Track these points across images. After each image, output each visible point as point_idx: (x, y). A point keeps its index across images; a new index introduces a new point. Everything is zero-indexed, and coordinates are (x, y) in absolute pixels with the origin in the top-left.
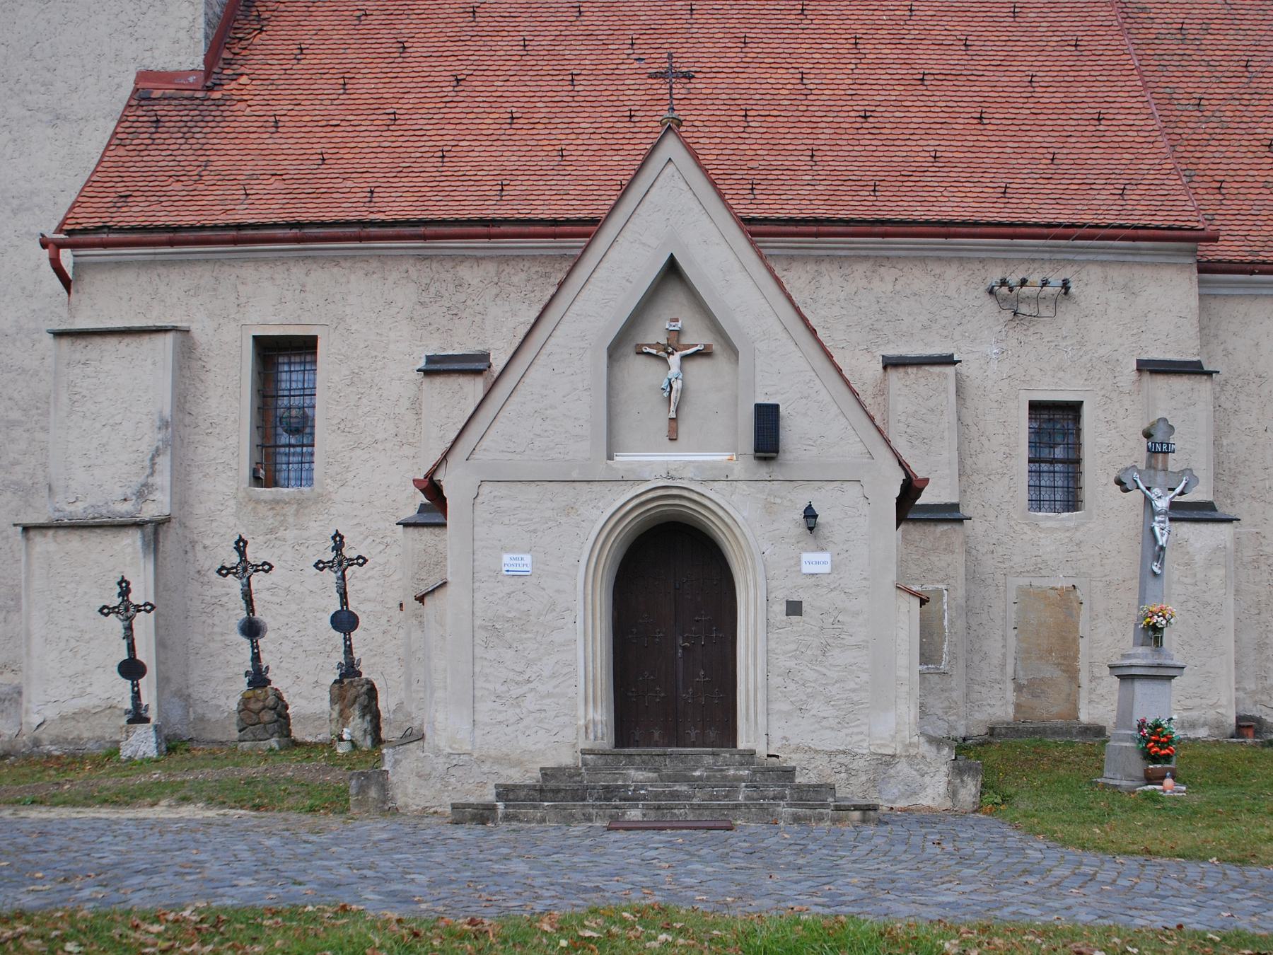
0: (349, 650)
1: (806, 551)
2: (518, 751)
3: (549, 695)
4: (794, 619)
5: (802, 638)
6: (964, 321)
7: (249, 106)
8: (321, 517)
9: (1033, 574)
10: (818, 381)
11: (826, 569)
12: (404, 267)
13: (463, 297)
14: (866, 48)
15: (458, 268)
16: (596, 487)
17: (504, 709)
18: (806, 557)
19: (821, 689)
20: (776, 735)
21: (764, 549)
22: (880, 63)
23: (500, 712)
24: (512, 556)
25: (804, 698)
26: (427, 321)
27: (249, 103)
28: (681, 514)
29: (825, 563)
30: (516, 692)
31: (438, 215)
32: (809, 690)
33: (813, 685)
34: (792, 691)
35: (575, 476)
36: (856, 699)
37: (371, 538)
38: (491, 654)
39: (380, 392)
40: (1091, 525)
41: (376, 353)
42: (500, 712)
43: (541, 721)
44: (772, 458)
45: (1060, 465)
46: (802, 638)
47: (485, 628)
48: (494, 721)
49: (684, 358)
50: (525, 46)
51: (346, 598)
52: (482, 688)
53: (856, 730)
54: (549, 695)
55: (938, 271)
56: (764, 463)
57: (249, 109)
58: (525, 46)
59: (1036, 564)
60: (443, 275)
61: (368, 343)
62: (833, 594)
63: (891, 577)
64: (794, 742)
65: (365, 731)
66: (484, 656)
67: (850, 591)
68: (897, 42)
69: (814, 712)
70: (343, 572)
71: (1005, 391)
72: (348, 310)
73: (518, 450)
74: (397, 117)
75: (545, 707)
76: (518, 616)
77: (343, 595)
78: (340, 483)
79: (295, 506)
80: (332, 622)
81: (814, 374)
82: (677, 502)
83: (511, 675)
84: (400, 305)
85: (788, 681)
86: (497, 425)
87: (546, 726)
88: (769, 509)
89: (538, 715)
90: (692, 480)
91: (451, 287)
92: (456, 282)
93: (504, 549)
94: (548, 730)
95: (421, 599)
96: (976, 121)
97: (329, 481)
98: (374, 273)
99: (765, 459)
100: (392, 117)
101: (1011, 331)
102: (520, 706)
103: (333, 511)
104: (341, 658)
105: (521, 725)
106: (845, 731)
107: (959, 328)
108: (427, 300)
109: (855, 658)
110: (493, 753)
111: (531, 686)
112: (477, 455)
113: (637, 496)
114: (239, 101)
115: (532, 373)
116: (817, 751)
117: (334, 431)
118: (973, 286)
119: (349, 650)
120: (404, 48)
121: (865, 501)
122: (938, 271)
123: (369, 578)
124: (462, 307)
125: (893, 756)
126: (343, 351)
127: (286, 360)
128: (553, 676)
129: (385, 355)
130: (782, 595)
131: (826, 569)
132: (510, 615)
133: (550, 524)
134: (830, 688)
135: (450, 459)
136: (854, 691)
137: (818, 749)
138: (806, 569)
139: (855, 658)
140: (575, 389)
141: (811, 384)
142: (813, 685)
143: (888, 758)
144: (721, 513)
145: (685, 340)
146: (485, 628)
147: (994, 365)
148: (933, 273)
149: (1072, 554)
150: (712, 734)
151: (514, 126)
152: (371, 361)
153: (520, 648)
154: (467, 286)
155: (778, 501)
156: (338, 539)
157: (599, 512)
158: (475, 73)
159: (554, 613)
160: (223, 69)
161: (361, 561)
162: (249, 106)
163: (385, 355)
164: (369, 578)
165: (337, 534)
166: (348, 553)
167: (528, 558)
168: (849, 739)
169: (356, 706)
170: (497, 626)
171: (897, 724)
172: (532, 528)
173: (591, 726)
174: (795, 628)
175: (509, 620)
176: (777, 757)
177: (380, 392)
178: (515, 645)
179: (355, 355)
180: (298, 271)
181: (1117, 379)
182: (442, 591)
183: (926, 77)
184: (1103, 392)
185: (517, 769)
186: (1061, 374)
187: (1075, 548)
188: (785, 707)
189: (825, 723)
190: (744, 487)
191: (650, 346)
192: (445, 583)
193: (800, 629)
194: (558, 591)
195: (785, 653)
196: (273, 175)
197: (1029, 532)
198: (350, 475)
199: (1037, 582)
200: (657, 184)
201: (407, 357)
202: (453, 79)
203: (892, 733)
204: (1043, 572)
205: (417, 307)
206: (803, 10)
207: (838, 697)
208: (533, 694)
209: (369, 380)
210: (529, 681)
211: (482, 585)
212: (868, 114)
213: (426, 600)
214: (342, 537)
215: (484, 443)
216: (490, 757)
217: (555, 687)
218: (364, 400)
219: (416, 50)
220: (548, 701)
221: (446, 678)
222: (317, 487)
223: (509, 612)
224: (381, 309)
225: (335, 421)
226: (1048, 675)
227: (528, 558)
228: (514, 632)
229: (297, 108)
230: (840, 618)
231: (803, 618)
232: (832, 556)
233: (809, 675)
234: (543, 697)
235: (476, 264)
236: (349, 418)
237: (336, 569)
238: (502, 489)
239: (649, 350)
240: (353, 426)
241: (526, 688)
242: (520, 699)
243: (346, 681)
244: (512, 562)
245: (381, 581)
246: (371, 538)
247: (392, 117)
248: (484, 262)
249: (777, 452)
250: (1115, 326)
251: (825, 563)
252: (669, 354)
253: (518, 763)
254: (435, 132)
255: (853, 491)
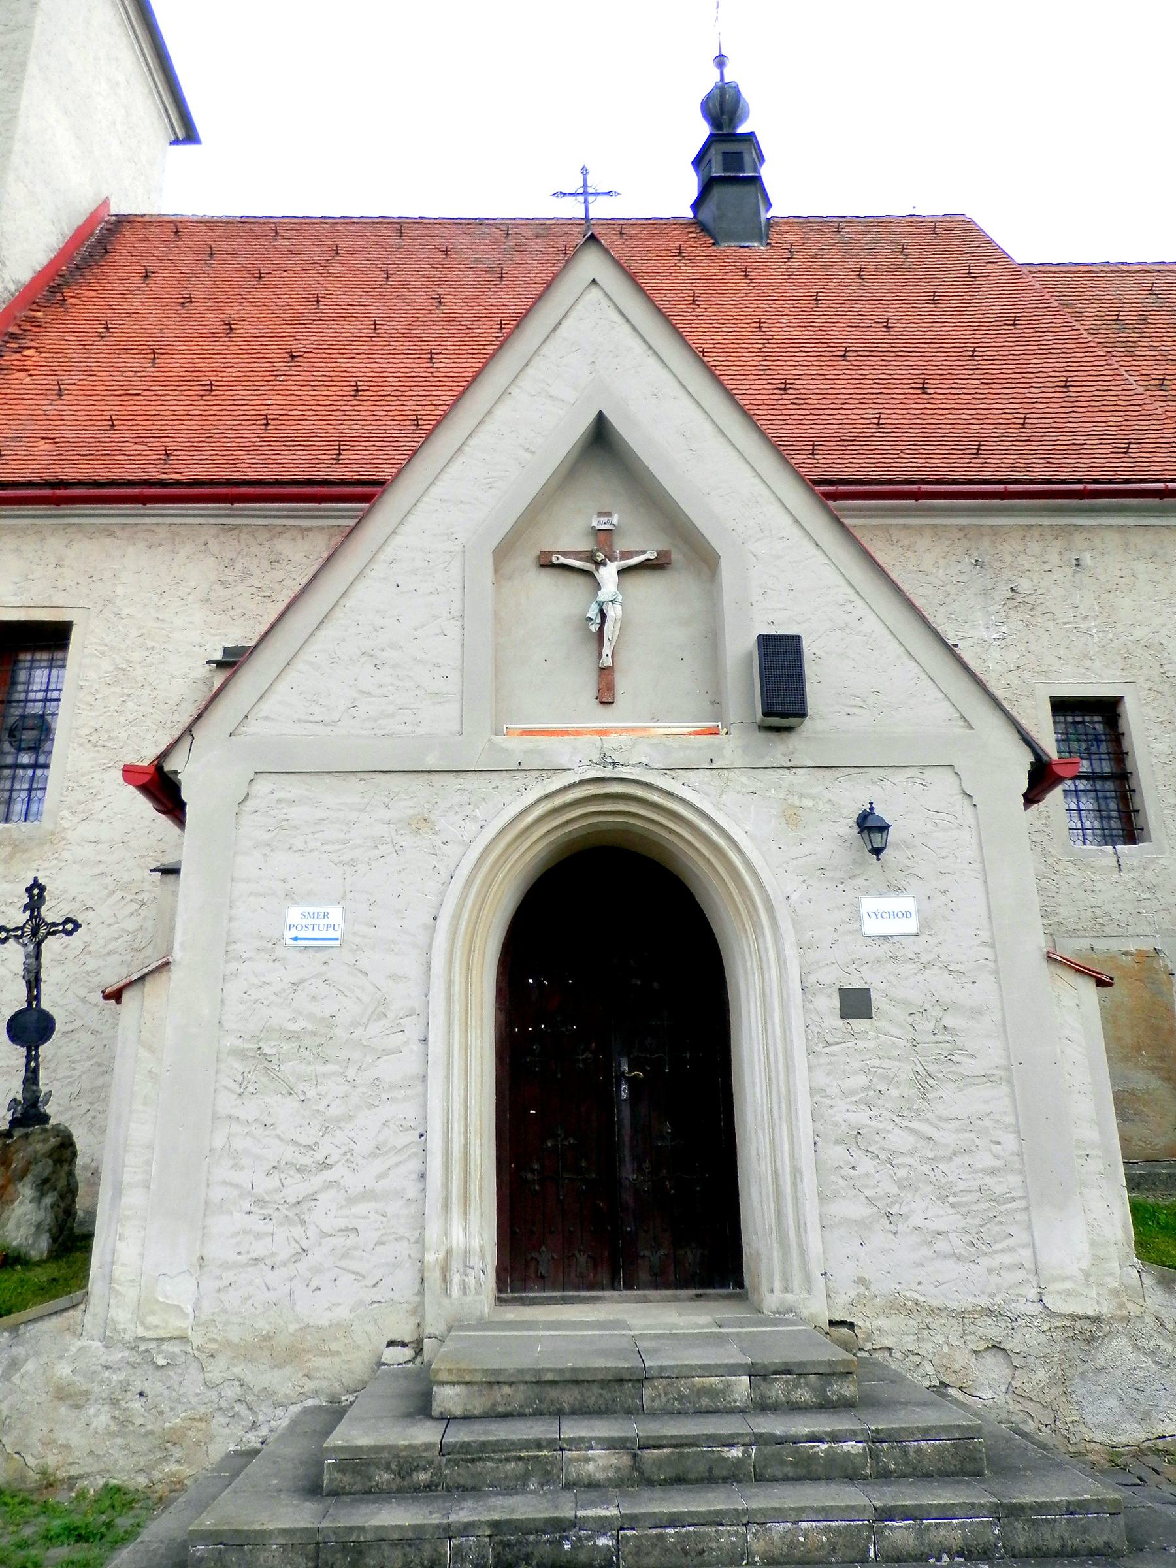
0: (31, 1077)
1: (866, 892)
2: (292, 1328)
3: (367, 1195)
4: (859, 1024)
5: (876, 1062)
6: (948, 600)
7: (30, 375)
8: (46, 864)
9: (1093, 933)
10: (859, 603)
11: (910, 926)
12: (203, 539)
13: (280, 575)
14: (770, 329)
15: (275, 541)
16: (471, 781)
17: (268, 1227)
18: (869, 904)
19: (926, 1169)
20: (845, 1273)
21: (788, 890)
22: (790, 343)
23: (259, 1236)
24: (306, 910)
25: (894, 1190)
26: (230, 604)
27: (31, 372)
28: (626, 832)
29: (906, 915)
30: (297, 1188)
31: (251, 475)
32: (902, 1173)
33: (909, 1160)
34: (867, 1175)
35: (431, 762)
36: (999, 1190)
37: (120, 894)
38: (250, 1110)
39: (154, 694)
40: (1162, 862)
41: (153, 644)
42: (259, 1236)
43: (345, 1255)
44: (789, 729)
45: (1085, 782)
46: (876, 1062)
47: (240, 1054)
48: (243, 1259)
49: (622, 572)
50: (375, 329)
51: (38, 987)
52: (225, 1183)
53: (1007, 1259)
54: (367, 1195)
55: (906, 542)
56: (772, 736)
57: (29, 378)
58: (375, 329)
59: (1095, 918)
60: (255, 549)
61: (144, 631)
62: (928, 972)
63: (1038, 942)
64: (884, 1286)
65: (38, 1226)
66: (235, 1112)
67: (960, 968)
68: (807, 324)
69: (917, 1220)
70: (38, 945)
71: (1015, 686)
72: (120, 590)
73: (327, 719)
74: (214, 388)
75: (355, 1223)
76: (310, 1027)
77: (34, 982)
78: (83, 816)
79: (9, 849)
80: (10, 1028)
81: (850, 591)
82: (621, 807)
83: (289, 1153)
84: (193, 584)
85: (857, 1153)
86: (291, 676)
87: (355, 1266)
88: (792, 817)
89: (338, 1241)
90: (649, 768)
91: (265, 563)
92: (273, 558)
93: (290, 896)
94: (359, 1275)
95: (116, 996)
96: (919, 391)
97: (65, 813)
98: (160, 545)
99: (778, 730)
100: (209, 388)
101: (1013, 611)
102: (303, 1223)
103: (66, 855)
104: (15, 1088)
105: (303, 1266)
106: (985, 1262)
107: (942, 609)
108: (231, 579)
109: (986, 1102)
110: (234, 1336)
111: (328, 1175)
112: (253, 727)
113: (547, 797)
114: (18, 371)
115: (360, 590)
116: (934, 1312)
117: (81, 745)
118: (954, 558)
119: (31, 1077)
120: (231, 329)
121: (966, 802)
122: (906, 542)
123: (109, 953)
124: (278, 587)
125: (1096, 1320)
126: (107, 640)
127: (29, 657)
128: (378, 1151)
129: (165, 646)
130: (835, 977)
131: (910, 926)
132: (293, 1027)
133: (383, 849)
134: (944, 1167)
135: (199, 733)
136: (993, 1172)
137: (934, 1303)
138: (872, 927)
139: (986, 1102)
140: (435, 617)
141: (849, 607)
142: (909, 1160)
143: (1086, 1326)
144: (705, 826)
145: (620, 545)
146: (240, 1054)
147: (995, 654)
148: (900, 544)
149: (1143, 904)
150: (691, 1255)
151: (358, 398)
152: (147, 653)
153: (311, 1094)
154: (286, 562)
155: (807, 803)
156: (36, 891)
157: (475, 827)
158: (314, 351)
159: (383, 1022)
160: (7, 342)
161: (69, 926)
162: (30, 375)
163: (165, 646)
164: (109, 953)
165: (36, 884)
166: (51, 912)
167: (336, 915)
168: (994, 1279)
169: (29, 1178)
170: (267, 1050)
171: (1093, 1244)
172: (346, 857)
173: (456, 1264)
174: (861, 1044)
175: (292, 1037)
176: (851, 1325)
177: (154, 694)
178: (300, 1087)
179: (123, 646)
180: (55, 543)
181: (1166, 668)
182: (164, 976)
183: (848, 354)
184: (1149, 685)
185: (288, 1370)
186: (1088, 663)
187: (1147, 895)
188: (856, 1209)
189: (942, 1245)
190: (744, 779)
191: (565, 554)
192: (167, 964)
193: (871, 1044)
194: (394, 977)
195: (845, 1095)
196: (43, 438)
197: (1077, 873)
198: (98, 805)
199: (1101, 945)
200: (573, 315)
201: (197, 647)
202: (287, 355)
203: (1085, 1265)
204: (1108, 930)
205: (218, 587)
206: (694, 301)
207: (962, 1185)
208: (332, 1192)
209: (140, 679)
210: (325, 1165)
211: (244, 967)
212: (788, 386)
213: (126, 997)
214: (42, 889)
215: (266, 707)
216: (229, 1343)
217: (380, 1177)
218: (130, 704)
219: (241, 331)
220: (361, 1208)
221: (149, 1163)
222: (46, 823)
223: (293, 1020)
224: (166, 588)
225: (85, 731)
226: (1141, 1086)
227: (336, 915)
228: (301, 1060)
229: (91, 378)
230: (948, 1021)
231: (877, 1022)
232: (918, 903)
233: (899, 1140)
234: (351, 1201)
235: (300, 536)
236: (106, 727)
237: (25, 940)
238: (293, 788)
239: (563, 560)
240: (110, 738)
241: (318, 1180)
242: (305, 1206)
243: (18, 1133)
244: (305, 922)
245: (128, 958)
246: (120, 894)
247: (209, 388)
248: (310, 534)
249: (803, 715)
250: (1150, 602)
251: (906, 915)
252: (602, 564)
253: (292, 1354)
254: (259, 402)
255: (942, 785)
